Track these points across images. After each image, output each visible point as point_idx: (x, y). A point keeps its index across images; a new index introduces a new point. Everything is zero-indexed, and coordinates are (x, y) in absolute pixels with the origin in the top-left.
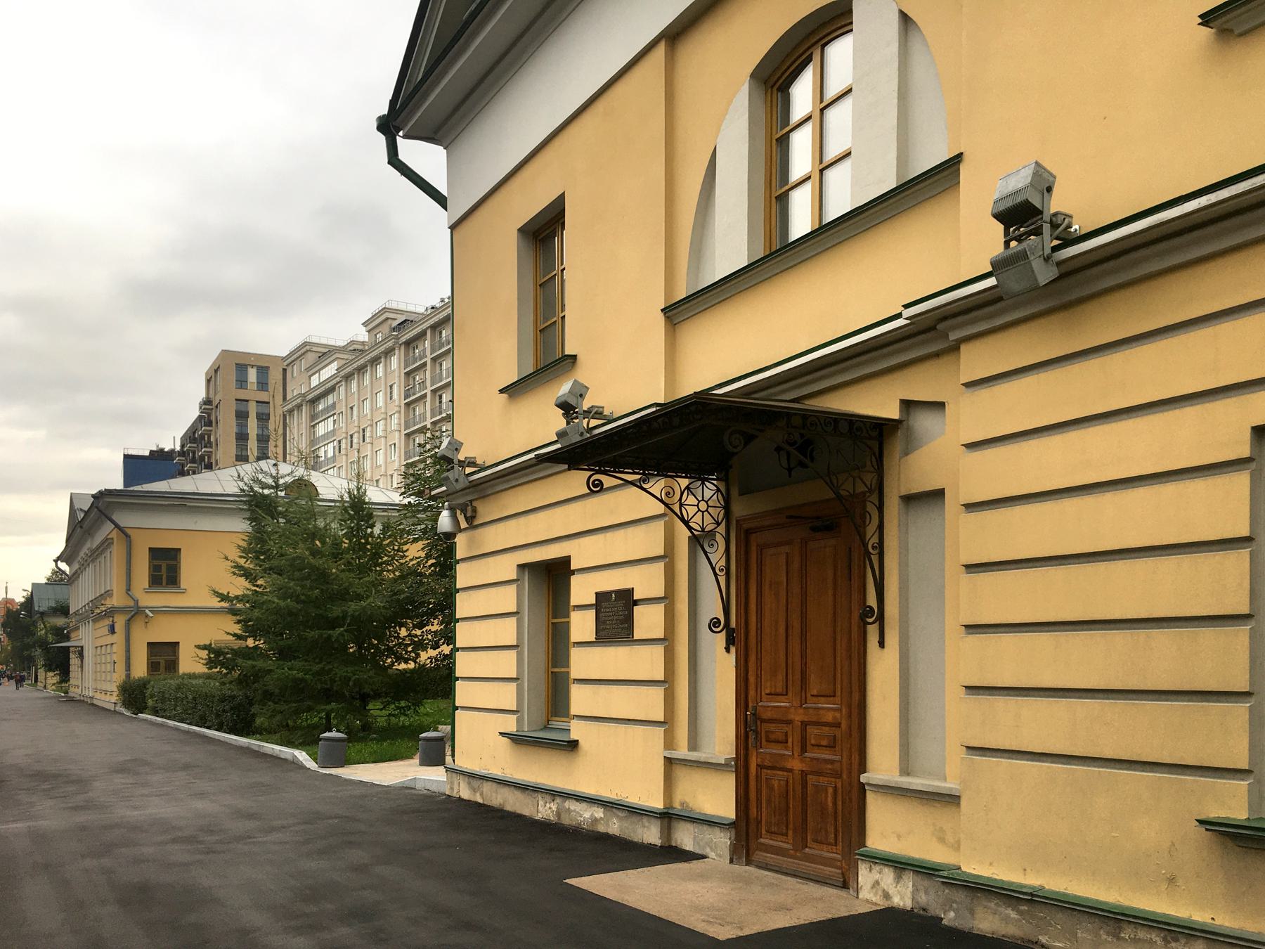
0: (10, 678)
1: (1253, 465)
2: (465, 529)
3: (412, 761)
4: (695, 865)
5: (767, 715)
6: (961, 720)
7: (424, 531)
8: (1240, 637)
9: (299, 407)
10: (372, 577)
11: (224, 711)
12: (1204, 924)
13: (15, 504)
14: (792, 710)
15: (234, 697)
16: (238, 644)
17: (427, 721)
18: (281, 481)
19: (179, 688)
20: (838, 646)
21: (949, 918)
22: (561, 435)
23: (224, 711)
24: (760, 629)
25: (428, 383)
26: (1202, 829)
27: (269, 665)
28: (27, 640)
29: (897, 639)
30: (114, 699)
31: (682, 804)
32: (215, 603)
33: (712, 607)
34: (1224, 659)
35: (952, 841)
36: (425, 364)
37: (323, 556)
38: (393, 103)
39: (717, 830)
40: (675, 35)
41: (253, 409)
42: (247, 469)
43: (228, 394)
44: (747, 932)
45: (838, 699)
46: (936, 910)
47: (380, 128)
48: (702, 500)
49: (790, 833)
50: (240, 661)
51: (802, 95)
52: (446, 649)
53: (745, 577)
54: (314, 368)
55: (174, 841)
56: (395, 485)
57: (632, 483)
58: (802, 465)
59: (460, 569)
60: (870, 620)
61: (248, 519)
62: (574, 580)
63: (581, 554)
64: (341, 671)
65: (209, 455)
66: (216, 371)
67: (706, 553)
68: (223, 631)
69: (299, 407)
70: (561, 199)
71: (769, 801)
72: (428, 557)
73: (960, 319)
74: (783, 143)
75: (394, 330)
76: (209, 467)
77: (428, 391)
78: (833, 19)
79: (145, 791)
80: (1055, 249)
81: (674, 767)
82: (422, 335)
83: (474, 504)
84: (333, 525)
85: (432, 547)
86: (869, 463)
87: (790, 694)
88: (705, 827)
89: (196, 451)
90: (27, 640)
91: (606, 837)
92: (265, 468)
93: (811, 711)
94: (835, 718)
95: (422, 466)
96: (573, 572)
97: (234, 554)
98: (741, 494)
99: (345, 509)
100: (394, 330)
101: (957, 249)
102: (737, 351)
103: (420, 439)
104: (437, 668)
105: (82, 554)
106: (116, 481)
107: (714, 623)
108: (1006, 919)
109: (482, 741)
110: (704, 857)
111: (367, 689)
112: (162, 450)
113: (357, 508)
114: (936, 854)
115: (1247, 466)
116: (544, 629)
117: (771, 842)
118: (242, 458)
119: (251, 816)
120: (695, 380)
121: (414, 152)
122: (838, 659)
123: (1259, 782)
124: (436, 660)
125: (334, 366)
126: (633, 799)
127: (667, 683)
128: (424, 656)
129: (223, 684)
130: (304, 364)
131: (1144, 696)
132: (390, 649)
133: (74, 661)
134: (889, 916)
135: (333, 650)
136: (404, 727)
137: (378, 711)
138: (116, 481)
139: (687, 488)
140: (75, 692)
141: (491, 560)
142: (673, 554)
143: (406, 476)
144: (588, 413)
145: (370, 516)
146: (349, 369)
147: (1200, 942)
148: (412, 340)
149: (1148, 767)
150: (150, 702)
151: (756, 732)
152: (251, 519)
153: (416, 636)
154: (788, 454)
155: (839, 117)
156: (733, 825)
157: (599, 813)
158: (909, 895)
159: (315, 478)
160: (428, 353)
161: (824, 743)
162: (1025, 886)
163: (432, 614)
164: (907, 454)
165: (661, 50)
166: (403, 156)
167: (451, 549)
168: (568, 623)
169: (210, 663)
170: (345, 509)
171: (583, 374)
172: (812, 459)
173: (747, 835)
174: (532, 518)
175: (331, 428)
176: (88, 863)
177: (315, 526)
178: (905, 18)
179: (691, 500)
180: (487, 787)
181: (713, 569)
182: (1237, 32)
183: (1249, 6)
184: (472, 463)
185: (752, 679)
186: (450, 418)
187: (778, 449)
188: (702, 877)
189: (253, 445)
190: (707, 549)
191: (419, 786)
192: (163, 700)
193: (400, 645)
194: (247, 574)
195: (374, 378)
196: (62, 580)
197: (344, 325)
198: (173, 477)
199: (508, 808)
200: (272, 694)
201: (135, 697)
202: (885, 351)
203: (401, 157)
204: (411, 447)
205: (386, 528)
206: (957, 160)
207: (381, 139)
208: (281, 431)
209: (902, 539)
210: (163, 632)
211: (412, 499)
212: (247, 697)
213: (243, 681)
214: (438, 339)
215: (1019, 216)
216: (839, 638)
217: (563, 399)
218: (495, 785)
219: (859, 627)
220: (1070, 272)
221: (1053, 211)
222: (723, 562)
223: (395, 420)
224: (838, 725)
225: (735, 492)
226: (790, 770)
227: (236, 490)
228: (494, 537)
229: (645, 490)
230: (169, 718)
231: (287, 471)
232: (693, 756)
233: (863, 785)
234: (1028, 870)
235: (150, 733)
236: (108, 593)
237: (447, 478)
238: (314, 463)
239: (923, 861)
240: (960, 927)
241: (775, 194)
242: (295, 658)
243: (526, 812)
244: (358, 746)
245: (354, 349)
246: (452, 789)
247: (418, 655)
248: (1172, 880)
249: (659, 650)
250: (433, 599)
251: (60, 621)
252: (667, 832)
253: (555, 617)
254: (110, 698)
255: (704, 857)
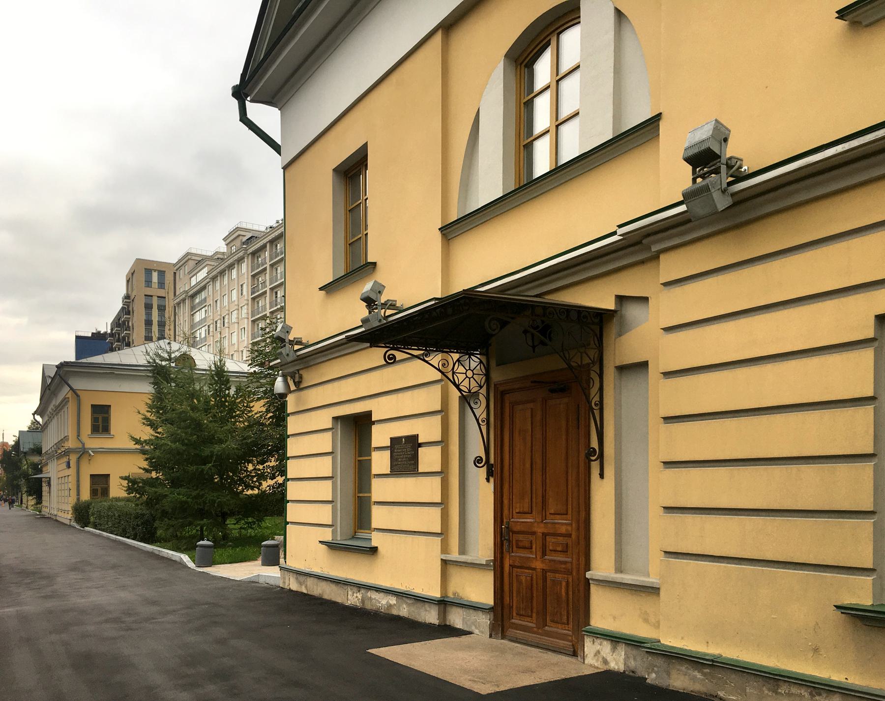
0: (5, 501)
1: (876, 344)
2: (294, 391)
3: (256, 562)
4: (464, 639)
5: (517, 528)
6: (659, 533)
7: (265, 392)
8: (867, 470)
9: (184, 300)
10: (228, 427)
11: (137, 525)
12: (840, 682)
13: (8, 372)
14: (536, 524)
15: (143, 515)
16: (146, 476)
17: (267, 532)
18: (173, 356)
19: (109, 508)
20: (570, 478)
21: (652, 678)
22: (365, 321)
23: (137, 525)
24: (512, 464)
25: (268, 283)
26: (839, 612)
27: (166, 491)
28: (16, 473)
29: (613, 472)
30: (70, 516)
31: (454, 594)
32: (132, 445)
33: (476, 448)
34: (854, 486)
35: (653, 621)
36: (265, 269)
37: (199, 410)
38: (243, 76)
39: (480, 613)
40: (449, 26)
41: (155, 302)
42: (152, 346)
43: (140, 291)
44: (502, 688)
45: (569, 516)
46: (641, 672)
47: (234, 95)
48: (469, 370)
49: (534, 615)
50: (147, 488)
51: (543, 71)
52: (280, 479)
53: (500, 426)
54: (193, 272)
55: (107, 621)
56: (245, 359)
57: (417, 357)
58: (543, 343)
59: (291, 420)
60: (593, 458)
61: (152, 383)
62: (375, 429)
63: (379, 409)
64: (210, 496)
65: (128, 336)
66: (132, 274)
67: (471, 408)
68: (136, 466)
69: (184, 300)
70: (365, 147)
71: (518, 592)
72: (268, 411)
73: (660, 236)
74: (529, 105)
75: (244, 243)
76: (128, 345)
77: (268, 289)
78: (565, 15)
79: (89, 584)
80: (730, 184)
81: (448, 566)
82: (263, 247)
83: (301, 372)
84: (205, 388)
85: (270, 404)
86: (592, 342)
87: (534, 513)
88: (471, 611)
89: (118, 336)
90: (16, 473)
91: (398, 619)
92: (163, 346)
93: (549, 525)
94: (567, 530)
95: (263, 344)
96: (374, 423)
97: (144, 409)
98: (498, 365)
99: (212, 376)
100: (244, 243)
101: (659, 183)
102: (493, 260)
103: (262, 324)
104: (274, 493)
105: (50, 409)
106: (70, 356)
107: (478, 460)
108: (694, 679)
109: (307, 548)
110: (470, 633)
111: (226, 510)
112: (99, 332)
113: (220, 375)
114: (642, 631)
115: (871, 344)
116: (353, 465)
117: (520, 622)
118: (149, 339)
119: (154, 603)
120: (462, 282)
121: (259, 112)
122: (570, 487)
123: (880, 577)
124: (273, 488)
125: (206, 270)
126: (418, 590)
127: (443, 504)
128: (265, 485)
129: (137, 505)
130: (187, 269)
131: (796, 514)
132: (241, 479)
133: (45, 488)
134: (607, 677)
135: (203, 480)
136: (250, 537)
137: (233, 526)
138: (70, 356)
139: (458, 360)
140: (45, 511)
141: (313, 413)
142: (448, 410)
143: (252, 351)
144: (384, 305)
145: (228, 381)
146: (214, 273)
147: (837, 695)
148: (257, 251)
149: (798, 567)
150: (92, 519)
151: (509, 540)
152: (154, 384)
153: (259, 470)
154: (533, 335)
155: (571, 87)
156: (492, 609)
157: (393, 600)
158: (622, 661)
159: (194, 353)
160: (268, 261)
161: (559, 549)
162: (708, 655)
163: (270, 454)
164: (620, 335)
165: (439, 36)
166: (250, 115)
167: (284, 406)
168: (370, 460)
169: (129, 490)
170: (212, 376)
171: (381, 276)
172: (550, 339)
173: (502, 617)
174: (343, 382)
175: (203, 316)
176: (54, 637)
177: (194, 389)
178: (619, 13)
179: (461, 369)
180: (310, 581)
181: (477, 420)
182: (864, 24)
183: (873, 5)
184: (299, 342)
185: (506, 502)
186: (283, 309)
187: (525, 332)
188: (469, 648)
189: (155, 328)
190: (473, 405)
191: (261, 581)
192: (100, 517)
193: (248, 476)
194: (152, 425)
195: (230, 279)
196: (37, 428)
197: (211, 243)
198: (106, 352)
199: (326, 597)
200: (167, 513)
201: (83, 515)
202: (604, 259)
203: (249, 116)
204: (256, 330)
205: (238, 390)
206: (658, 118)
207: (235, 102)
208: (172, 319)
209: (617, 400)
210: (100, 466)
211: (257, 369)
212: (152, 515)
213: (149, 503)
214: (274, 250)
215: (703, 160)
216: (570, 471)
217: (366, 295)
218: (316, 580)
219: (585, 463)
220: (741, 201)
221: (728, 156)
222: (484, 415)
223: (245, 310)
224: (570, 536)
225: (493, 363)
226: (534, 569)
227: (144, 362)
228: (315, 397)
229: (427, 362)
230: (103, 530)
231: (177, 348)
232: (463, 558)
233: (588, 580)
234: (710, 643)
235: (92, 542)
236: (66, 438)
237: (281, 353)
238: (192, 342)
239: (632, 636)
240: (660, 685)
241: (523, 143)
242: (181, 486)
243: (339, 600)
244: (220, 551)
245: (218, 258)
246: (284, 582)
247: (261, 484)
248: (816, 650)
249: (437, 481)
250: (270, 442)
251: (36, 459)
252: (443, 614)
253: (360, 456)
254: (67, 517)
255: (470, 633)
